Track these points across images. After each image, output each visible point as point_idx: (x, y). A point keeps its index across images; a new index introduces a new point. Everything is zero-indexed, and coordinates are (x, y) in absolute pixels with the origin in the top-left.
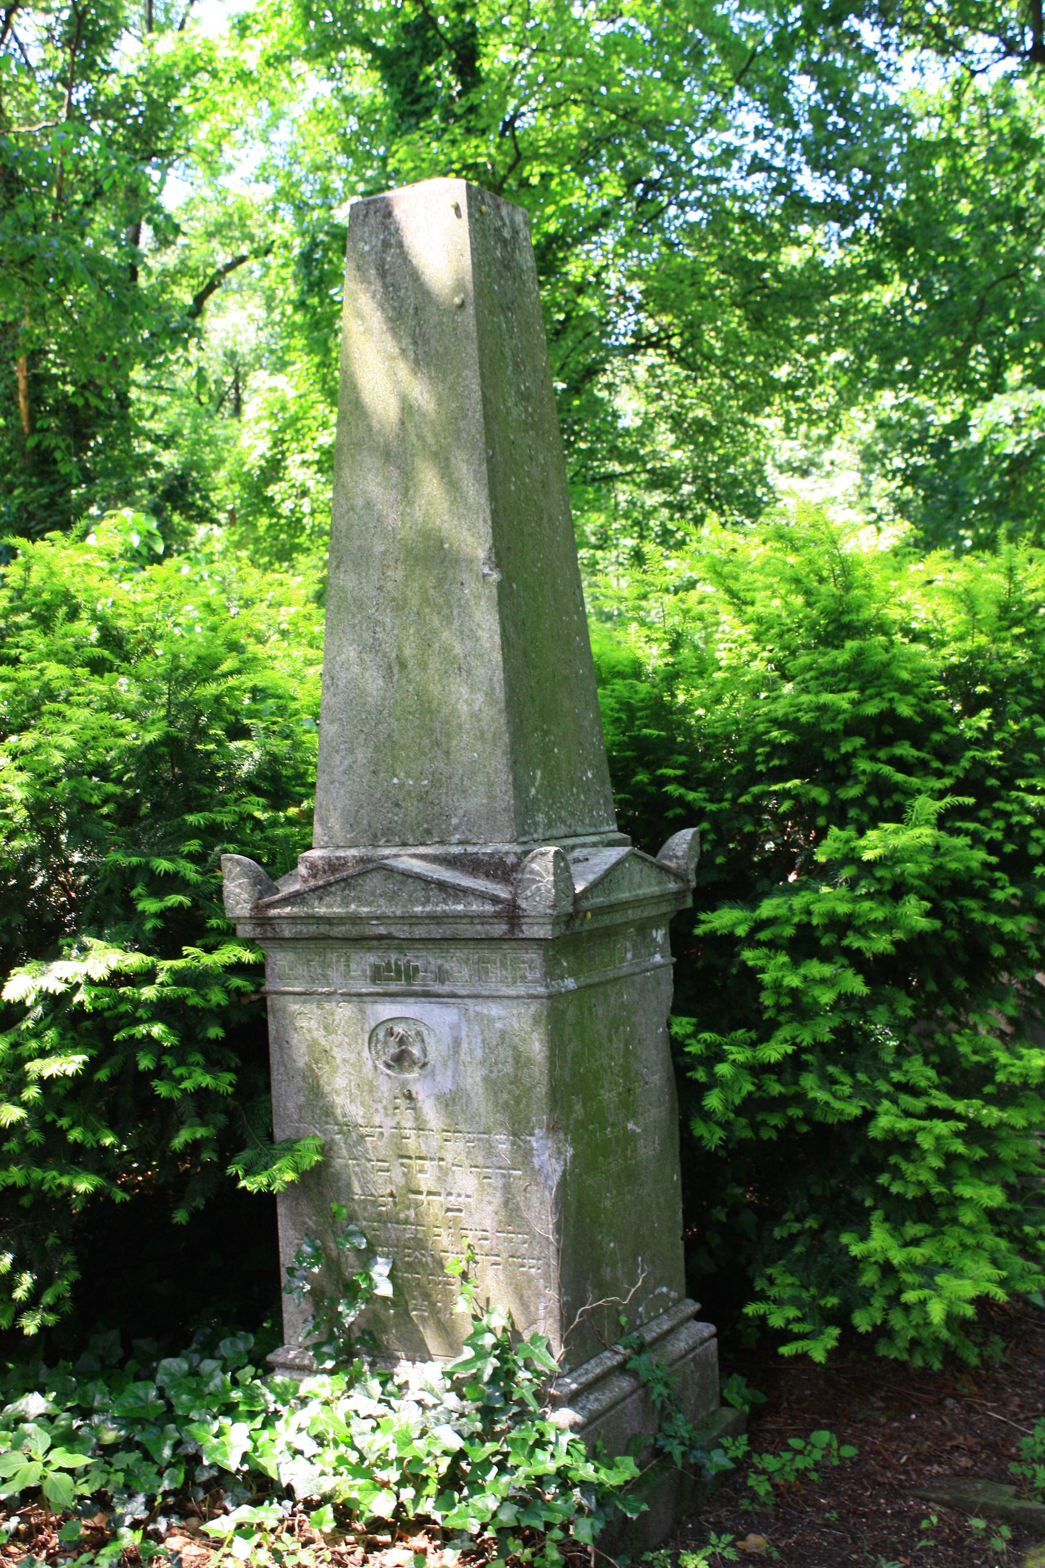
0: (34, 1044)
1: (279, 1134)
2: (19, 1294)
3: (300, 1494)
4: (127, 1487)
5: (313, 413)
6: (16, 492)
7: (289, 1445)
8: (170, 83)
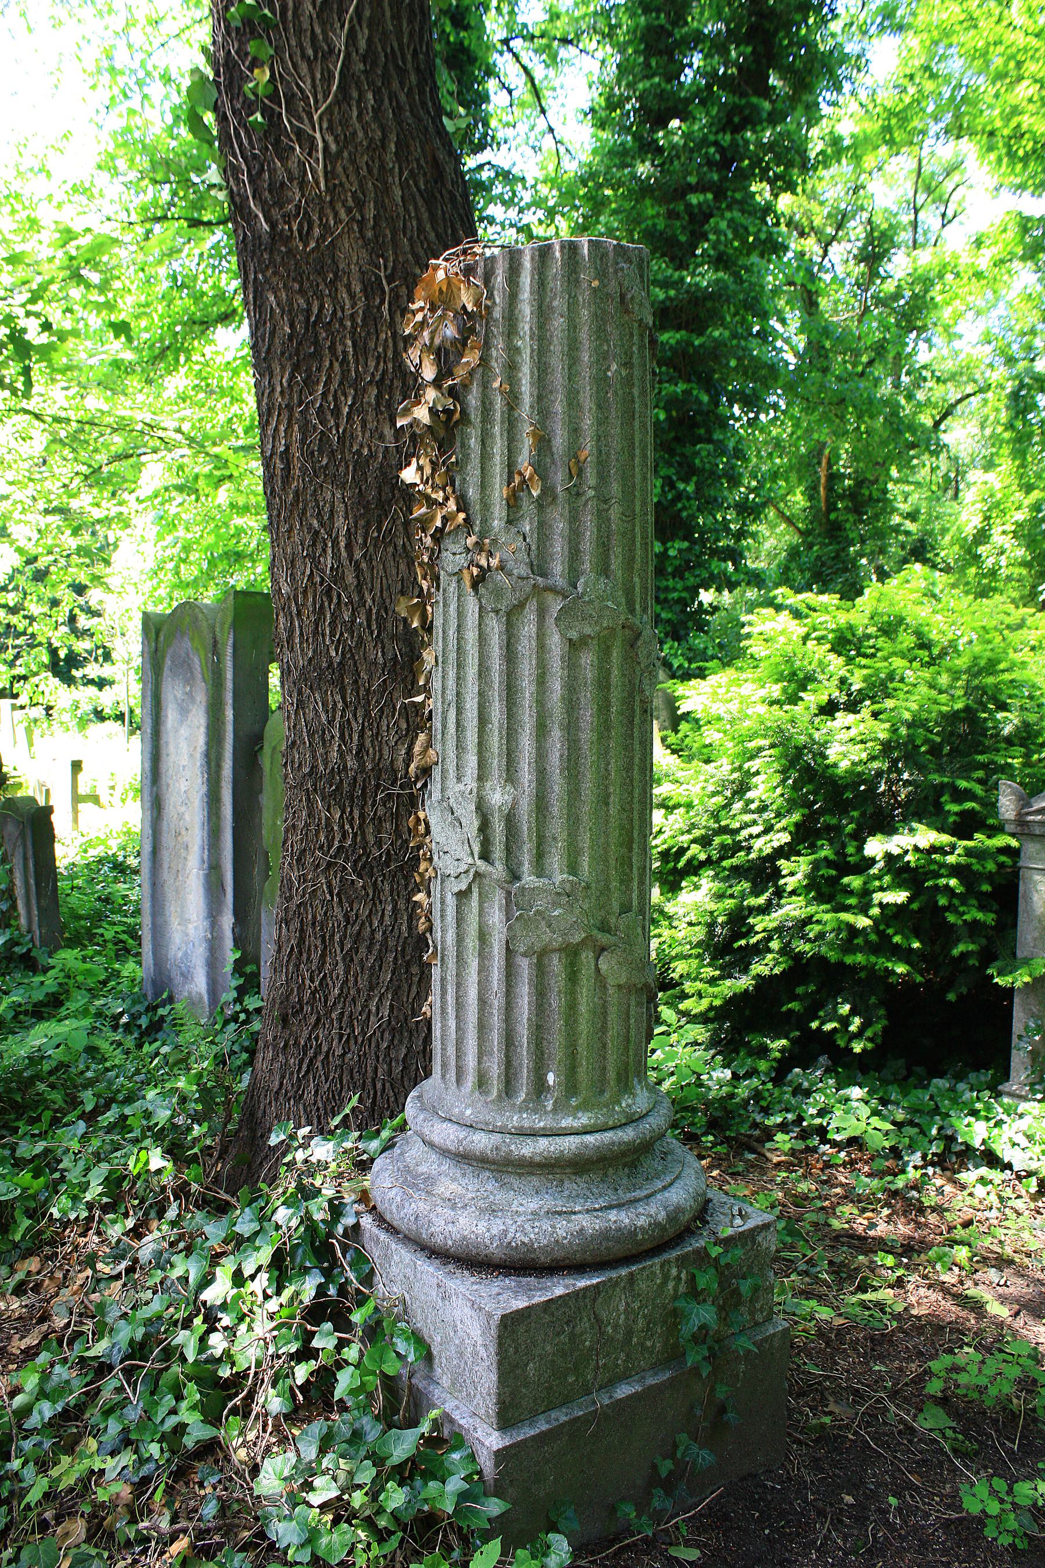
0: (877, 883)
1: (1019, 954)
2: (853, 1028)
3: (1015, 1169)
4: (910, 1146)
5: (1012, 499)
6: (815, 548)
7: (1010, 1139)
8: (927, 282)
